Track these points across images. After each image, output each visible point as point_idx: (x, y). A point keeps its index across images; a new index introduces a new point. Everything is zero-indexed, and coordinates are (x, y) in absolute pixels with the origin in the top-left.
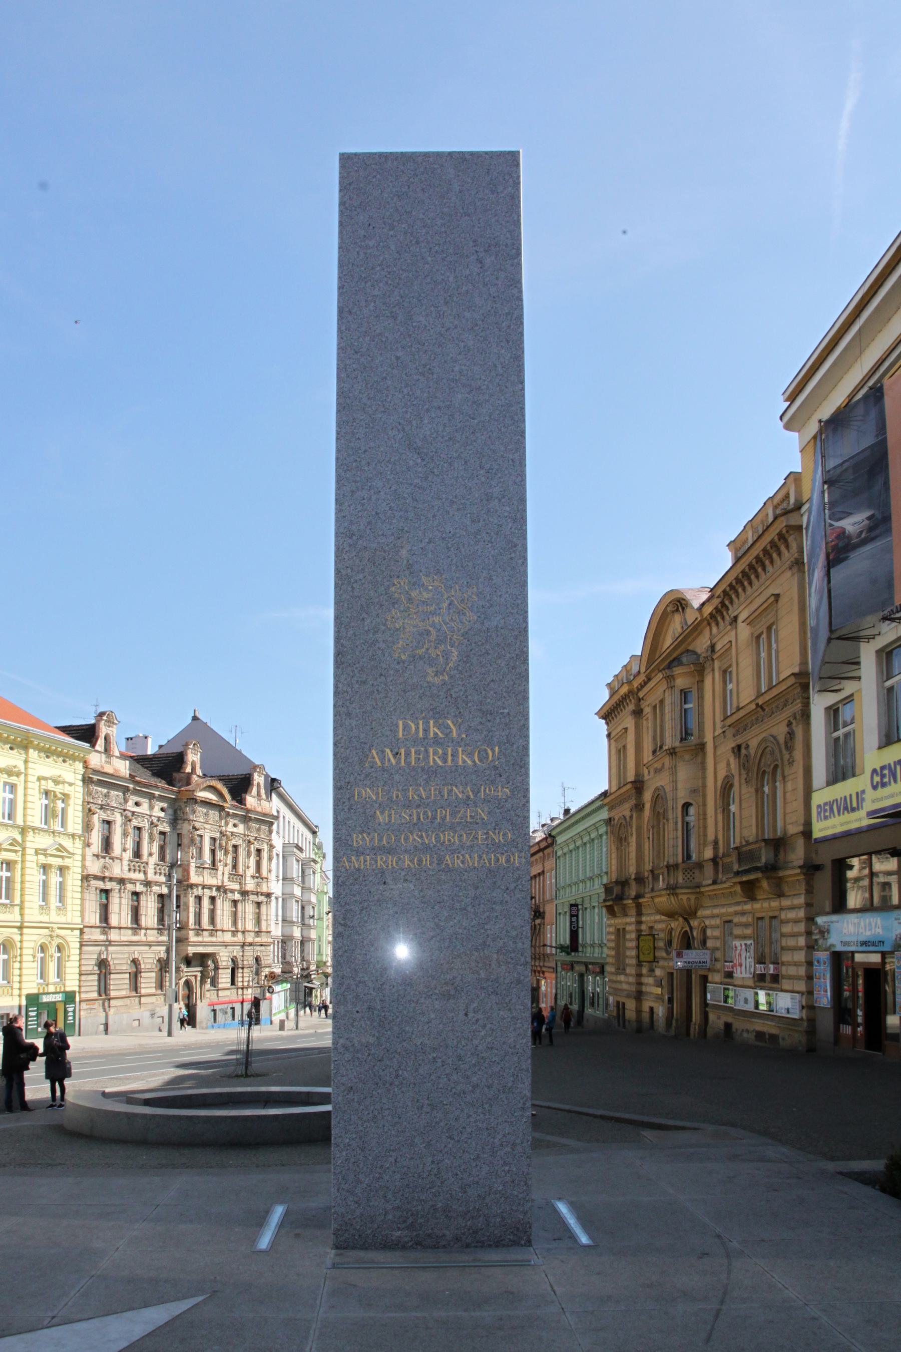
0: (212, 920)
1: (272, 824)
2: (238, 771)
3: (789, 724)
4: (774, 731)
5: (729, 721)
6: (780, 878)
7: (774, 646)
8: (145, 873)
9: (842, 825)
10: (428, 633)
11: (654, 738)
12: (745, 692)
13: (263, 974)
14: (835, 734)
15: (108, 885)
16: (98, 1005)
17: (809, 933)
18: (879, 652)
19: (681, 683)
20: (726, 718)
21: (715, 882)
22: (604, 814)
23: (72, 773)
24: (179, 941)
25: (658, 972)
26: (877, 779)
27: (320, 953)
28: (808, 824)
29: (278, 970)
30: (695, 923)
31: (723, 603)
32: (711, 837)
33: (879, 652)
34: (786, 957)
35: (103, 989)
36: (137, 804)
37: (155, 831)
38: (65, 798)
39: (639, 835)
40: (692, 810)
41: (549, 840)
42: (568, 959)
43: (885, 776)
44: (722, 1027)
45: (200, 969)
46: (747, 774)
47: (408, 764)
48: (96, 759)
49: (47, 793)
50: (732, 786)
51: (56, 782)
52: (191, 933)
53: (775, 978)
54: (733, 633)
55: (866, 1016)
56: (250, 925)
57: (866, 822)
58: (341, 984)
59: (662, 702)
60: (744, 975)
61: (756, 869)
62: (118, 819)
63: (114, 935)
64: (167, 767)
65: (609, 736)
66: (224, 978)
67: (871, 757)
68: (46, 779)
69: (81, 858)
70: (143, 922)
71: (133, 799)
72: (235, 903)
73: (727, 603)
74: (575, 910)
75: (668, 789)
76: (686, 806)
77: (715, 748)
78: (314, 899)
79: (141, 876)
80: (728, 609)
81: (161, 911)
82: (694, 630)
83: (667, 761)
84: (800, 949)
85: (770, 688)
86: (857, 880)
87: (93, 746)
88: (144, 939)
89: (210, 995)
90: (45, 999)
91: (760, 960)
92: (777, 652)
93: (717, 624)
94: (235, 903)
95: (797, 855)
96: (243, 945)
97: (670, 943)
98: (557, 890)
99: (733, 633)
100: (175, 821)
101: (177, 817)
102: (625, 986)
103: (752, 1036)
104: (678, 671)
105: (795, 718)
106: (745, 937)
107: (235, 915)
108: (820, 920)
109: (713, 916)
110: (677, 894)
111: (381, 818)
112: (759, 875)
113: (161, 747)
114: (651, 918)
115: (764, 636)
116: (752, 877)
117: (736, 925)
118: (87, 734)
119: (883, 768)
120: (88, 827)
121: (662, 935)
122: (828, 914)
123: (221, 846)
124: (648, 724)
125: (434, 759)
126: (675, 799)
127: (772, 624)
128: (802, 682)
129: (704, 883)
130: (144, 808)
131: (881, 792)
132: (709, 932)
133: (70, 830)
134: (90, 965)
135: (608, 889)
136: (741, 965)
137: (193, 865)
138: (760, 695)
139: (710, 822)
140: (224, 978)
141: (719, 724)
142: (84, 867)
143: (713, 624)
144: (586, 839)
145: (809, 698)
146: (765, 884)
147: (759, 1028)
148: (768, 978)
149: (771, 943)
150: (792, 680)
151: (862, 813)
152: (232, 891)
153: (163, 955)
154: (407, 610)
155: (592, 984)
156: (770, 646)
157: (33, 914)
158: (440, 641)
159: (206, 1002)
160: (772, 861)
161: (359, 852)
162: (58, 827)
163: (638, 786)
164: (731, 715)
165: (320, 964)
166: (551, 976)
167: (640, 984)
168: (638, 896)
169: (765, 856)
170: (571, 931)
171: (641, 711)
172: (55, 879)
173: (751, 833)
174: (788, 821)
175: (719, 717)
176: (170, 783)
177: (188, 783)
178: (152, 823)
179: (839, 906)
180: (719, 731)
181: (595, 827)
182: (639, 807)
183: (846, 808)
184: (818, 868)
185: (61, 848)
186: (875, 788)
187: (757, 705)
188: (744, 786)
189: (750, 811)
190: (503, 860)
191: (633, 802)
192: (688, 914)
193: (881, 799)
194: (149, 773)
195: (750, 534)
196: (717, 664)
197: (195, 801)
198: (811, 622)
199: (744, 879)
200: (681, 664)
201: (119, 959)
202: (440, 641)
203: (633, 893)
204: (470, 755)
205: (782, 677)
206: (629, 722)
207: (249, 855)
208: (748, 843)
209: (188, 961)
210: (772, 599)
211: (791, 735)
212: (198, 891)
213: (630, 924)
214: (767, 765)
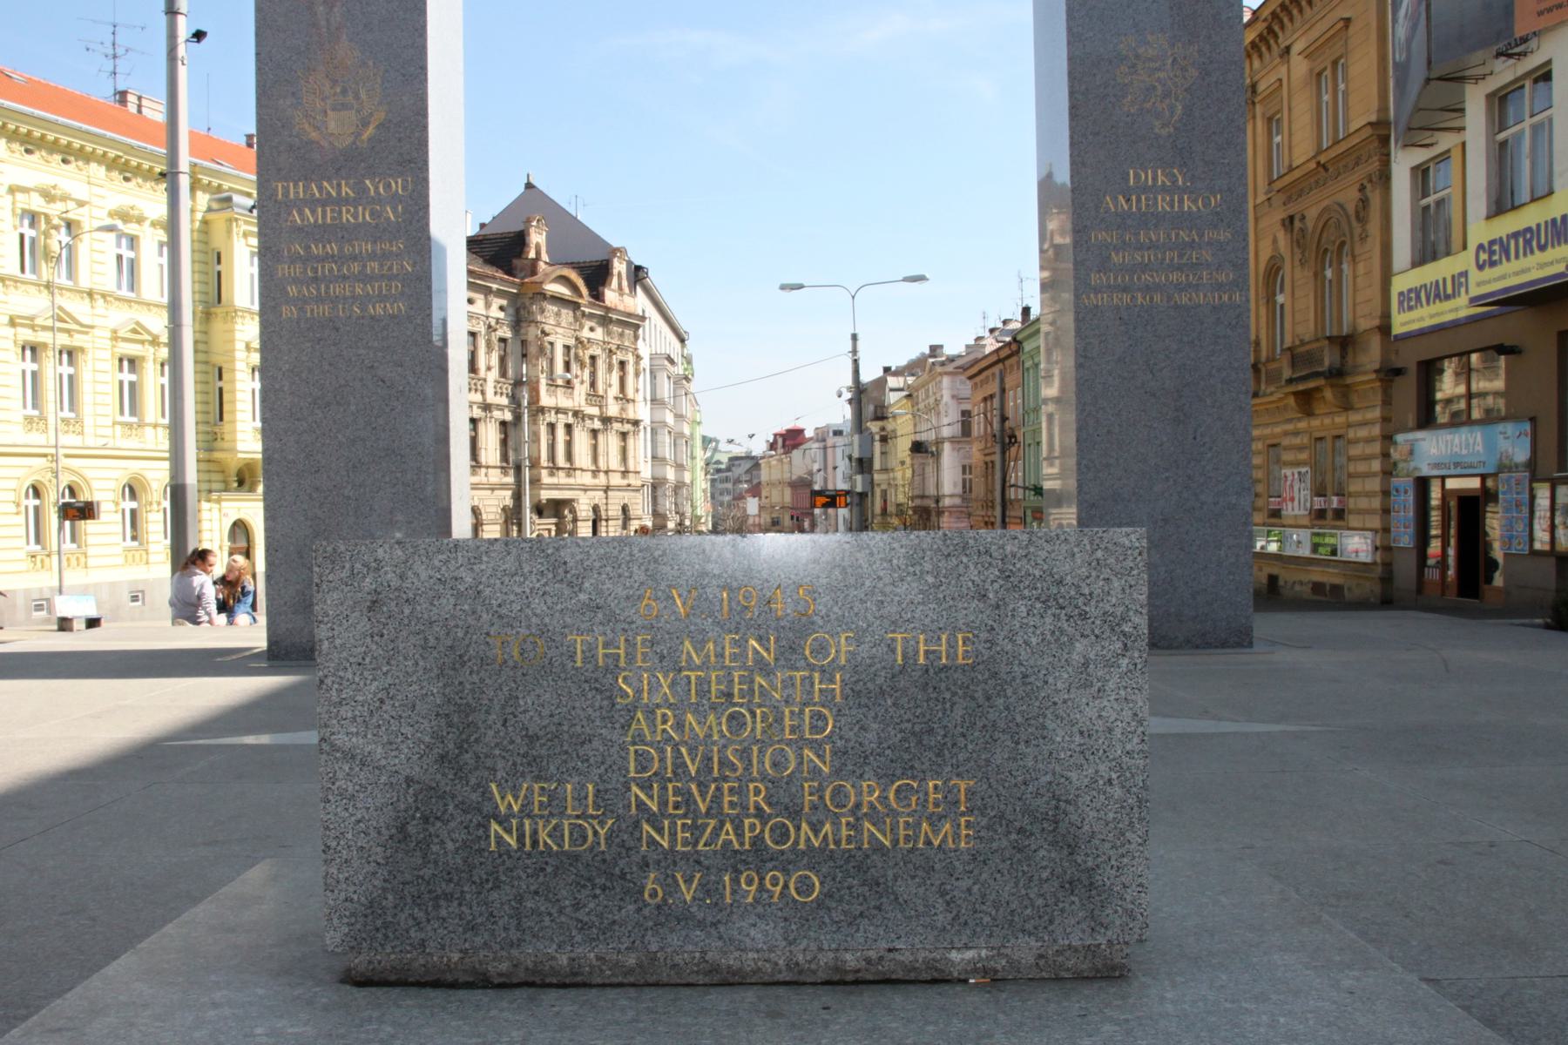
0: (569, 456)
1: (637, 327)
2: (596, 256)
3: (1362, 189)
4: (1340, 198)
5: (1278, 185)
6: (1347, 386)
7: (1342, 86)
8: (483, 393)
9: (1432, 316)
10: (1154, 88)
12: (1300, 144)
13: (633, 528)
14: (1424, 202)
17: (1386, 455)
18: (1490, 97)
20: (1271, 183)
24: (531, 482)
26: (1484, 256)
28: (1386, 316)
29: (649, 524)
31: (1270, 30)
33: (1490, 97)
34: (1355, 486)
37: (494, 339)
41: (1014, 347)
43: (1493, 253)
44: (1265, 581)
45: (554, 520)
46: (1303, 253)
47: (1139, 209)
52: (544, 473)
53: (1339, 514)
54: (1284, 69)
56: (615, 463)
57: (1463, 314)
58: (1083, 410)
60: (1296, 512)
61: (1317, 375)
67: (1481, 231)
70: (483, 459)
72: (594, 433)
73: (1276, 28)
77: (1256, 220)
78: (687, 431)
80: (1276, 37)
81: (504, 443)
84: (1374, 475)
85: (1336, 142)
88: (484, 480)
91: (1320, 491)
92: (1345, 93)
93: (1261, 56)
94: (594, 433)
95: (1371, 356)
96: (607, 489)
98: (1026, 412)
99: (1284, 69)
101: (520, 317)
103: (1307, 589)
105: (1370, 181)
106: (1298, 464)
108: (1400, 438)
111: (1116, 258)
112: (1321, 382)
113: (483, 226)
115: (1328, 72)
116: (1311, 384)
117: (1285, 449)
119: (1492, 243)
122: (1412, 430)
123: (576, 356)
125: (1162, 205)
127: (1340, 57)
128: (1380, 133)
131: (1489, 273)
136: (1292, 499)
137: (543, 381)
138: (1320, 152)
143: (1255, 57)
145: (1388, 155)
146: (1328, 394)
147: (1316, 578)
148: (1330, 515)
149: (1334, 470)
150: (1369, 131)
151: (1462, 300)
152: (591, 417)
153: (509, 502)
154: (1134, 66)
156: (1335, 86)
158: (1167, 95)
160: (1337, 365)
161: (1097, 291)
164: (1280, 177)
169: (1329, 359)
173: (1307, 330)
174: (1359, 312)
176: (510, 272)
177: (534, 272)
178: (490, 326)
179: (1426, 420)
180: (1261, 198)
183: (1437, 296)
184: (1398, 372)
186: (1480, 267)
187: (1318, 163)
188: (1298, 270)
189: (1306, 301)
190: (1226, 298)
193: (1489, 282)
194: (480, 261)
196: (1259, 109)
197: (543, 296)
198: (1395, 55)
199: (1301, 387)
202: (1167, 95)
204: (1195, 201)
205: (1354, 127)
207: (610, 368)
208: (1303, 343)
209: (539, 510)
210: (1341, 24)
211: (1364, 202)
212: (551, 417)
214: (1333, 236)
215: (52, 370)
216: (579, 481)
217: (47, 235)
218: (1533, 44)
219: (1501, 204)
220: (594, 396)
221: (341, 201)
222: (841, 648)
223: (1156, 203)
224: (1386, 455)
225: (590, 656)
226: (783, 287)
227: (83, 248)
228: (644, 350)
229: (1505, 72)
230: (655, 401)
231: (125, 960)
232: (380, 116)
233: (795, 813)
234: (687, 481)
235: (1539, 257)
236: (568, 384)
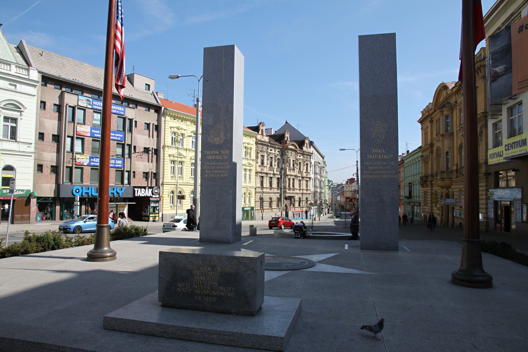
0: (293, 186)
2: (300, 139)
11: (437, 130)
15: (263, 175)
16: (260, 211)
17: (486, 194)
18: (508, 108)
19: (445, 113)
20: (461, 125)
21: (457, 177)
22: (420, 154)
23: (252, 141)
24: (284, 192)
25: (438, 206)
26: (507, 148)
27: (325, 197)
28: (487, 160)
29: (313, 202)
30: (450, 190)
31: (459, 88)
32: (455, 162)
33: (508, 108)
35: (262, 206)
36: (271, 150)
38: (251, 149)
39: (432, 161)
40: (449, 154)
42: (408, 201)
43: (509, 147)
48: (259, 137)
49: (245, 147)
51: (248, 144)
55: (505, 221)
56: (305, 188)
57: (501, 161)
59: (439, 119)
62: (266, 155)
63: (265, 190)
64: (278, 138)
65: (422, 128)
66: (297, 204)
67: (506, 141)
69: (255, 167)
71: (270, 148)
72: (300, 180)
74: (410, 185)
75: (441, 147)
76: (447, 153)
78: (323, 180)
79: (272, 172)
81: (278, 183)
82: (450, 96)
83: (441, 138)
86: (503, 178)
89: (293, 209)
90: (245, 209)
94: (300, 180)
96: (303, 194)
97: (442, 196)
100: (282, 155)
101: (283, 153)
102: (427, 210)
104: (444, 109)
107: (300, 184)
108: (490, 190)
109: (456, 188)
114: (435, 188)
118: (256, 129)
119: (508, 144)
120: (257, 157)
121: (439, 194)
124: (435, 125)
126: (443, 150)
130: (273, 151)
131: (508, 152)
132: (455, 193)
133: (252, 158)
134: (258, 199)
135: (421, 178)
140: (297, 204)
141: (458, 127)
142: (256, 169)
144: (414, 162)
152: (299, 177)
153: (279, 196)
155: (416, 209)
158: (381, 134)
159: (291, 211)
161: (365, 175)
162: (249, 158)
163: (432, 145)
165: (326, 201)
166: (402, 206)
167: (432, 209)
168: (432, 181)
172: (248, 173)
175: (458, 124)
180: (458, 129)
182: (432, 152)
183: (499, 156)
184: (490, 174)
185: (250, 164)
186: (506, 150)
191: (430, 150)
196: (457, 107)
197: (288, 149)
200: (445, 107)
201: (266, 197)
203: (430, 180)
206: (429, 125)
207: (304, 166)
209: (286, 198)
215: (177, 166)
217: (178, 137)
218: (518, 96)
219: (512, 134)
220: (300, 172)
221: (216, 155)
222: (219, 269)
224: (486, 194)
225: (190, 268)
226: (340, 150)
227: (185, 140)
228: (313, 161)
229: (511, 103)
230: (315, 173)
231: (138, 301)
232: (224, 138)
233: (213, 290)
234: (323, 191)
235: (520, 148)
236: (294, 169)
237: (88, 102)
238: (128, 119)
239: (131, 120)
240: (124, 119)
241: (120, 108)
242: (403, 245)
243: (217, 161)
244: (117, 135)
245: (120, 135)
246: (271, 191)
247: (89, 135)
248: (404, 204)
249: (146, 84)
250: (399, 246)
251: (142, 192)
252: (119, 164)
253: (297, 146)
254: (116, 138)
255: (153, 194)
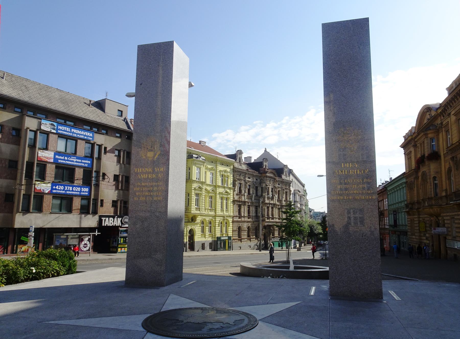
0: (272, 215)
19: (430, 136)
20: (448, 147)
22: (404, 180)
25: (427, 235)
30: (440, 218)
31: (445, 109)
32: (444, 188)
35: (239, 236)
39: (417, 187)
41: (385, 189)
48: (236, 165)
50: (451, 171)
52: (266, 219)
59: (423, 142)
62: (243, 182)
65: (405, 154)
68: (222, 171)
76: (435, 178)
87: (236, 161)
90: (222, 238)
97: (431, 225)
99: (449, 119)
102: (415, 240)
110: (433, 208)
117: (456, 219)
120: (234, 185)
126: (430, 175)
129: (443, 204)
132: (446, 222)
133: (229, 186)
134: (236, 228)
139: (444, 183)
141: (445, 150)
142: (234, 198)
157: (219, 212)
168: (418, 209)
170: (394, 220)
171: (417, 145)
175: (445, 147)
181: (401, 184)
182: (417, 178)
185: (226, 192)
192: (438, 216)
195: (454, 85)
196: (443, 129)
206: (412, 149)
213: (415, 218)
216: (275, 221)
221: (149, 173)
223: (350, 172)
224: (419, 226)
226: (318, 176)
228: (292, 189)
237: (52, 127)
238: (97, 145)
239: (100, 146)
240: (93, 145)
241: (89, 134)
242: (392, 292)
243: (152, 180)
244: (84, 161)
245: (87, 162)
246: (240, 220)
247: (52, 161)
248: (389, 234)
249: (118, 110)
250: (384, 290)
251: (110, 222)
252: (86, 192)
253: (276, 173)
254: (83, 165)
255: (122, 223)
